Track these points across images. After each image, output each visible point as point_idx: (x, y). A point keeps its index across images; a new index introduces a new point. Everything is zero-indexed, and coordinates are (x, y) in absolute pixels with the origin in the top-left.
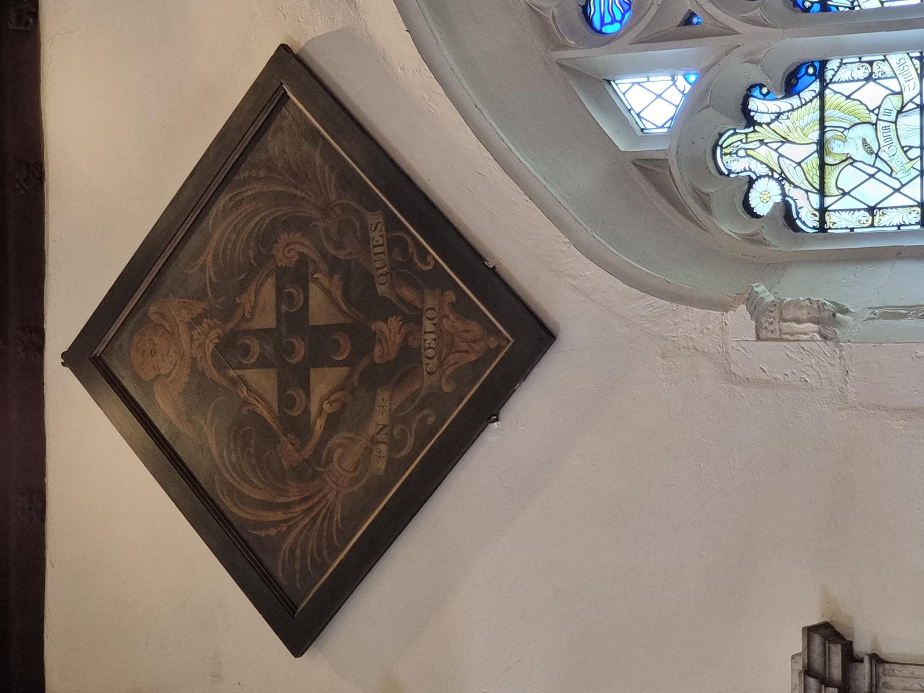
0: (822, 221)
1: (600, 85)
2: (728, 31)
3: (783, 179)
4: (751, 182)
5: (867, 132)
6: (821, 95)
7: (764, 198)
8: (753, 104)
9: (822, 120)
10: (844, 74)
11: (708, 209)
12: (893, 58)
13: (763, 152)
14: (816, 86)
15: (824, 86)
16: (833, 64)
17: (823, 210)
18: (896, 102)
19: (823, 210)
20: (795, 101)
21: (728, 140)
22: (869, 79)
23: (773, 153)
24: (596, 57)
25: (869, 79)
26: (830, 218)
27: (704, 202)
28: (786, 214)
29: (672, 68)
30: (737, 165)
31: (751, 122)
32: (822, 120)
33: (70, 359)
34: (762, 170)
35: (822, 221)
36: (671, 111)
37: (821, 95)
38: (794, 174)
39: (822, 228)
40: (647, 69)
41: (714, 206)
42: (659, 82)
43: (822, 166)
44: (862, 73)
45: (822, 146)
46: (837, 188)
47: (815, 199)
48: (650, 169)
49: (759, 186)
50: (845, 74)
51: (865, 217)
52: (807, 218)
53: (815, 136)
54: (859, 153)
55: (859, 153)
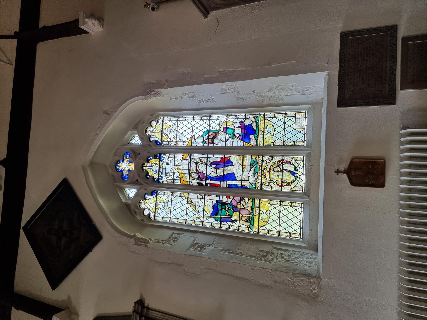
0: (155, 218)
1: (122, 190)
2: (142, 185)
3: (149, 210)
4: (144, 209)
5: (163, 204)
6: (156, 196)
7: (146, 212)
8: (146, 196)
9: (156, 200)
10: (160, 193)
11: (136, 214)
12: (168, 192)
13: (147, 204)
14: (156, 195)
15: (157, 195)
16: (159, 191)
17: (155, 216)
18: (168, 199)
19: (155, 216)
20: (152, 197)
21: (142, 201)
22: (164, 195)
23: (148, 205)
24: (123, 185)
25: (164, 195)
26: (156, 218)
27: (135, 212)
28: (149, 215)
29: (134, 188)
30: (143, 206)
31: (145, 199)
32: (156, 200)
33: (23, 228)
34: (146, 207)
35: (155, 218)
36: (133, 195)
37: (156, 196)
38: (151, 209)
39: (154, 219)
40: (138, 145)
41: (137, 213)
42: (132, 190)
43: (155, 208)
44: (163, 194)
45: (156, 206)
46: (293, 164)
47: (154, 214)
48: (127, 206)
49: (146, 210)
50: (161, 194)
51: (161, 218)
52: (152, 217)
53: (155, 203)
54: (161, 207)
55: (161, 207)
